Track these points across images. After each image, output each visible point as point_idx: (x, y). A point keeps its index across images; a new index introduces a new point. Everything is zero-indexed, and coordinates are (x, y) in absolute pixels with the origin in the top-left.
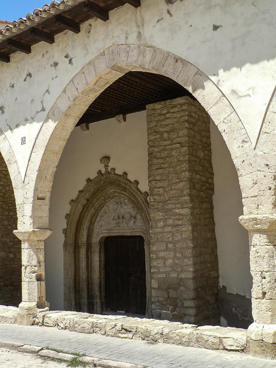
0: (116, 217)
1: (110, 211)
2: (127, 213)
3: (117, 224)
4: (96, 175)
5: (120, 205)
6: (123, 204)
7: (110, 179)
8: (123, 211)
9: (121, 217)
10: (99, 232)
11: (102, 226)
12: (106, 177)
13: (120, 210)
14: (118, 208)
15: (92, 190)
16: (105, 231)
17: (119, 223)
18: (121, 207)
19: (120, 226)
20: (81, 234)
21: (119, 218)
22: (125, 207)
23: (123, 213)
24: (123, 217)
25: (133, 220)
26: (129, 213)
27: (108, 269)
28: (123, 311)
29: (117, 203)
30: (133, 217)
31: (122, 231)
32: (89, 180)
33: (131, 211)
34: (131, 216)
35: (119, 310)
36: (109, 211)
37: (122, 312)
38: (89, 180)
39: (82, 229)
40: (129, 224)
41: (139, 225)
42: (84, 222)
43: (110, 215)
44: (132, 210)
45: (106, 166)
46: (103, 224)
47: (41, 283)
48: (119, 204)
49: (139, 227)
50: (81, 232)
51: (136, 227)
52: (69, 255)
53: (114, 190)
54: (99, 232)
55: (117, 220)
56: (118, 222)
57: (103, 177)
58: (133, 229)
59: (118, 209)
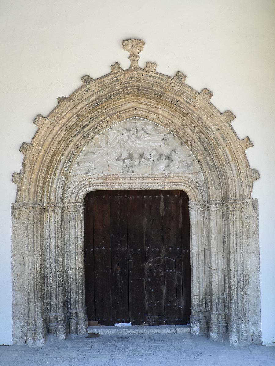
0: (125, 155)
1: (111, 144)
2: (150, 150)
3: (127, 169)
4: (107, 70)
5: (133, 134)
6: (142, 132)
7: (140, 82)
8: (141, 144)
9: (136, 156)
11: (88, 171)
12: (131, 78)
13: (134, 143)
14: (129, 138)
15: (92, 98)
16: (97, 181)
18: (136, 137)
19: (133, 172)
20: (48, 186)
21: (130, 156)
22: (146, 139)
23: (141, 148)
24: (142, 156)
25: (164, 162)
28: (128, 322)
29: (128, 131)
30: (163, 157)
31: (137, 181)
34: (161, 156)
35: (118, 322)
36: (107, 144)
37: (126, 325)
39: (51, 174)
40: (156, 169)
41: (178, 171)
42: (56, 160)
43: (109, 151)
45: (133, 56)
46: (93, 166)
48: (131, 133)
49: (180, 175)
50: (49, 181)
51: (170, 175)
52: (26, 225)
53: (134, 104)
55: (128, 161)
57: (123, 76)
58: (166, 177)
59: (129, 141)
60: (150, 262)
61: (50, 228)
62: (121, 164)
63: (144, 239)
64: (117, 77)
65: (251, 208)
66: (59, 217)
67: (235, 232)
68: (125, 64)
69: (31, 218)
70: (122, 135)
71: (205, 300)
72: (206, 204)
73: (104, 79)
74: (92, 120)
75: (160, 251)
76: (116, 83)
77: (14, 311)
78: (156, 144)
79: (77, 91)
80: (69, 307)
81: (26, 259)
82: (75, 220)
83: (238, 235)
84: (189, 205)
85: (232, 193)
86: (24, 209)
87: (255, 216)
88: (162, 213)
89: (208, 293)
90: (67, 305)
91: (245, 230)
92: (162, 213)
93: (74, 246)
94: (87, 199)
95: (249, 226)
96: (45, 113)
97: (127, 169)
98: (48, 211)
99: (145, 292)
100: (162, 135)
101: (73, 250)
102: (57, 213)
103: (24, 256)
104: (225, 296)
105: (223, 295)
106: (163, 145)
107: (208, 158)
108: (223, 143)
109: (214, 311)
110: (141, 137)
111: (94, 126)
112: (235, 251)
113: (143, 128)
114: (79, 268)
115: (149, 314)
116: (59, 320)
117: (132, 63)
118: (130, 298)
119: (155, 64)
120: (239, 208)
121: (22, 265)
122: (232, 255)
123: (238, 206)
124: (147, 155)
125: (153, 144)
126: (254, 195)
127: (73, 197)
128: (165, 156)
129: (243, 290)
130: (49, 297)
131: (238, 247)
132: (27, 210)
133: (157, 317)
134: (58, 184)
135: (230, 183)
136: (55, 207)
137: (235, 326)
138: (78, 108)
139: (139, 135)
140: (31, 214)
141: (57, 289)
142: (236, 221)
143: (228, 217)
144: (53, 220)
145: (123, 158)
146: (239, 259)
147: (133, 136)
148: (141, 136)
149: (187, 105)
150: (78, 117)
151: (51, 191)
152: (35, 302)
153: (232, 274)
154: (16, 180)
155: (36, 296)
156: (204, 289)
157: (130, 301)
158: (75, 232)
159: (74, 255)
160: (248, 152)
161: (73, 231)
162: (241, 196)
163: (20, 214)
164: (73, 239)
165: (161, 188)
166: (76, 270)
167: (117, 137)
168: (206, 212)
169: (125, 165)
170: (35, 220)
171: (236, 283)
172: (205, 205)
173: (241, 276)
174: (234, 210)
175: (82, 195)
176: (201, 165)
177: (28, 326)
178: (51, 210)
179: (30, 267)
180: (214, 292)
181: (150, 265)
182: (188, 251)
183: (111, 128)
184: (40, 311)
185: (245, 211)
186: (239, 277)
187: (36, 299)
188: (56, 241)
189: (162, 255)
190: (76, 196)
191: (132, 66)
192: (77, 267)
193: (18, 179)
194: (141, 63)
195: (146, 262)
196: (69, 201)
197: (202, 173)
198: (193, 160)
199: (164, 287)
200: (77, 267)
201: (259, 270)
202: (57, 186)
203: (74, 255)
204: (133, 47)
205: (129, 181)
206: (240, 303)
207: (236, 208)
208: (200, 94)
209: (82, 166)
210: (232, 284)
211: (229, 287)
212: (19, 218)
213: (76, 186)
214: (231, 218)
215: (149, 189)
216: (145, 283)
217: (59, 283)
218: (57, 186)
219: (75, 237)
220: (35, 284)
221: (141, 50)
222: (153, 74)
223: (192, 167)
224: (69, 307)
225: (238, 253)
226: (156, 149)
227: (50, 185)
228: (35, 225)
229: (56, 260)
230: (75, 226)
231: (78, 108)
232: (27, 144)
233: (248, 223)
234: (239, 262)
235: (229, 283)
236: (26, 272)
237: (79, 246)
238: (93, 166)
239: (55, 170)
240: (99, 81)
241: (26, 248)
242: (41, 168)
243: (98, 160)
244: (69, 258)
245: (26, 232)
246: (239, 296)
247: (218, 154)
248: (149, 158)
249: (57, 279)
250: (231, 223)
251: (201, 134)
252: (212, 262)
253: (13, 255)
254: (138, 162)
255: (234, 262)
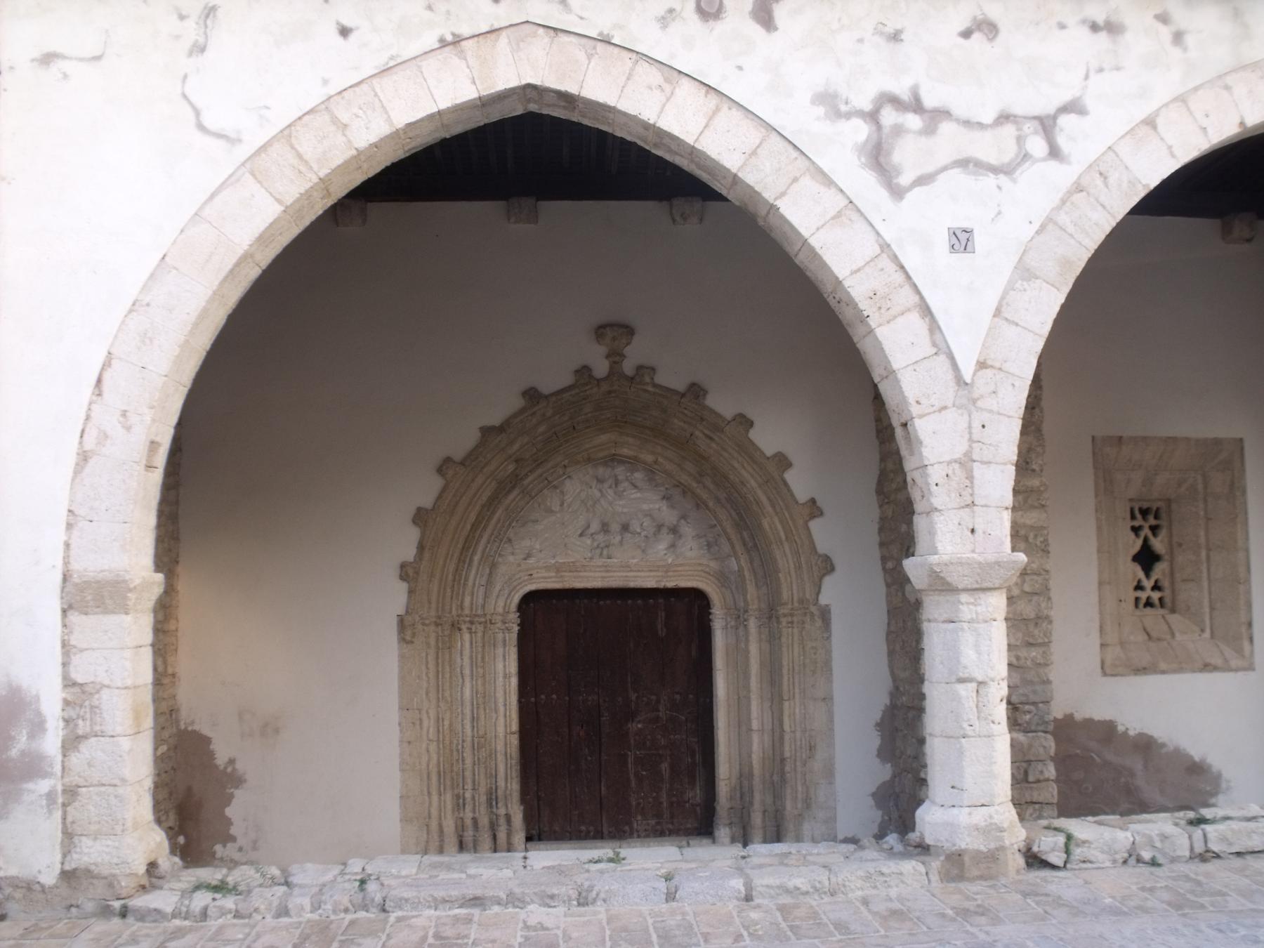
0: (595, 526)
1: (569, 506)
3: (598, 551)
4: (566, 379)
6: (626, 484)
9: (615, 527)
10: (518, 576)
11: (528, 556)
12: (610, 392)
13: (611, 504)
14: (603, 495)
17: (607, 546)
18: (615, 493)
19: (609, 557)
21: (605, 528)
22: (632, 496)
23: (625, 513)
24: (625, 528)
26: (649, 514)
27: (533, 699)
30: (665, 530)
32: (532, 395)
33: (659, 509)
36: (562, 505)
38: (532, 395)
41: (689, 554)
44: (664, 506)
45: (615, 356)
46: (538, 546)
47: (983, 503)
48: (606, 485)
52: (424, 655)
54: (514, 575)
55: (601, 538)
56: (602, 545)
57: (595, 390)
59: (603, 502)
60: (639, 722)
61: (462, 659)
62: (589, 542)
63: (629, 679)
64: (586, 391)
65: (819, 623)
66: (479, 639)
67: (791, 665)
68: (601, 368)
69: (433, 642)
70: (590, 490)
71: (741, 787)
72: (739, 617)
73: (564, 395)
74: (538, 465)
75: (658, 701)
76: (584, 402)
77: (404, 808)
78: (651, 506)
79: (515, 416)
80: (494, 803)
81: (424, 717)
82: (505, 645)
83: (797, 668)
84: (711, 617)
85: (785, 595)
86: (420, 627)
87: (825, 635)
88: (662, 632)
89: (745, 776)
90: (492, 799)
91: (807, 661)
92: (662, 632)
93: (502, 693)
94: (524, 606)
95: (815, 654)
96: (458, 455)
97: (598, 551)
98: (460, 629)
99: (632, 777)
100: (662, 489)
101: (501, 700)
102: (475, 632)
103: (420, 710)
104: (776, 778)
105: (772, 776)
106: (665, 508)
107: (745, 534)
108: (770, 509)
109: (757, 805)
110: (625, 493)
111: (541, 475)
112: (791, 697)
113: (627, 477)
114: (512, 733)
115: (639, 818)
116: (480, 825)
117: (611, 368)
118: (603, 788)
119: (653, 369)
120: (798, 622)
121: (418, 727)
122: (786, 704)
123: (795, 619)
124: (635, 526)
125: (645, 507)
126: (823, 600)
127: (501, 603)
128: (668, 528)
129: (805, 765)
130: (461, 785)
131: (797, 690)
132: (425, 628)
133: (653, 822)
134: (478, 579)
135: (782, 579)
136: (472, 623)
137: (791, 827)
138: (516, 446)
139: (620, 488)
140: (433, 636)
141: (476, 769)
142: (793, 645)
143: (780, 638)
144: (467, 645)
145: (592, 530)
146: (797, 711)
147: (610, 492)
148: (624, 491)
149: (708, 441)
150: (517, 461)
151: (464, 593)
152: (440, 791)
153: (787, 737)
154: (407, 575)
155: (442, 781)
156: (738, 767)
157: (603, 792)
158: (505, 666)
159: (502, 709)
160: (815, 525)
161: (500, 666)
162: (801, 601)
163: (414, 635)
164: (501, 679)
165: (661, 585)
166: (506, 737)
167: (579, 493)
168: (741, 628)
169: (595, 544)
170: (440, 644)
171: (793, 752)
172: (739, 617)
173: (801, 741)
174: (790, 625)
175: (516, 599)
176: (733, 547)
177: (428, 834)
178: (464, 627)
179: (431, 730)
180: (757, 771)
181: (640, 726)
182: (708, 700)
183: (569, 477)
184: (449, 806)
185: (807, 626)
186: (799, 743)
187: (442, 786)
188: (474, 682)
189: (661, 708)
190: (506, 601)
191: (611, 373)
192: (508, 730)
193: (411, 572)
194: (628, 367)
195: (633, 721)
196: (492, 611)
197: (733, 559)
198: (718, 535)
199: (665, 766)
200: (508, 730)
201: (832, 730)
202: (474, 584)
203: (502, 709)
204: (614, 339)
205: (604, 574)
206: (800, 789)
207: (792, 622)
208: (624, 79)
209: (517, 547)
210: (787, 754)
211: (783, 760)
212: (412, 642)
213: (506, 583)
214: (784, 640)
215: (638, 587)
216: (630, 760)
217: (479, 759)
218: (474, 584)
219: (505, 677)
220: (441, 759)
221: (628, 344)
222: (650, 388)
223: (716, 548)
224: (494, 803)
225: (797, 700)
226: (650, 515)
227: (462, 582)
228: (440, 654)
229: (473, 717)
230: (504, 656)
231: (516, 446)
232: (426, 510)
233: (813, 648)
234: (797, 717)
235: (782, 753)
236: (425, 737)
237: (513, 692)
238: (538, 546)
239: (472, 554)
240: (554, 399)
241: (424, 696)
242: (451, 552)
243: (546, 535)
244: (494, 715)
245: (424, 667)
246: (799, 776)
247: (737, 448)
248: (638, 530)
249: (476, 752)
250: (784, 649)
251: (733, 490)
252: (752, 718)
253: (401, 708)
254: (618, 538)
255: (790, 716)
